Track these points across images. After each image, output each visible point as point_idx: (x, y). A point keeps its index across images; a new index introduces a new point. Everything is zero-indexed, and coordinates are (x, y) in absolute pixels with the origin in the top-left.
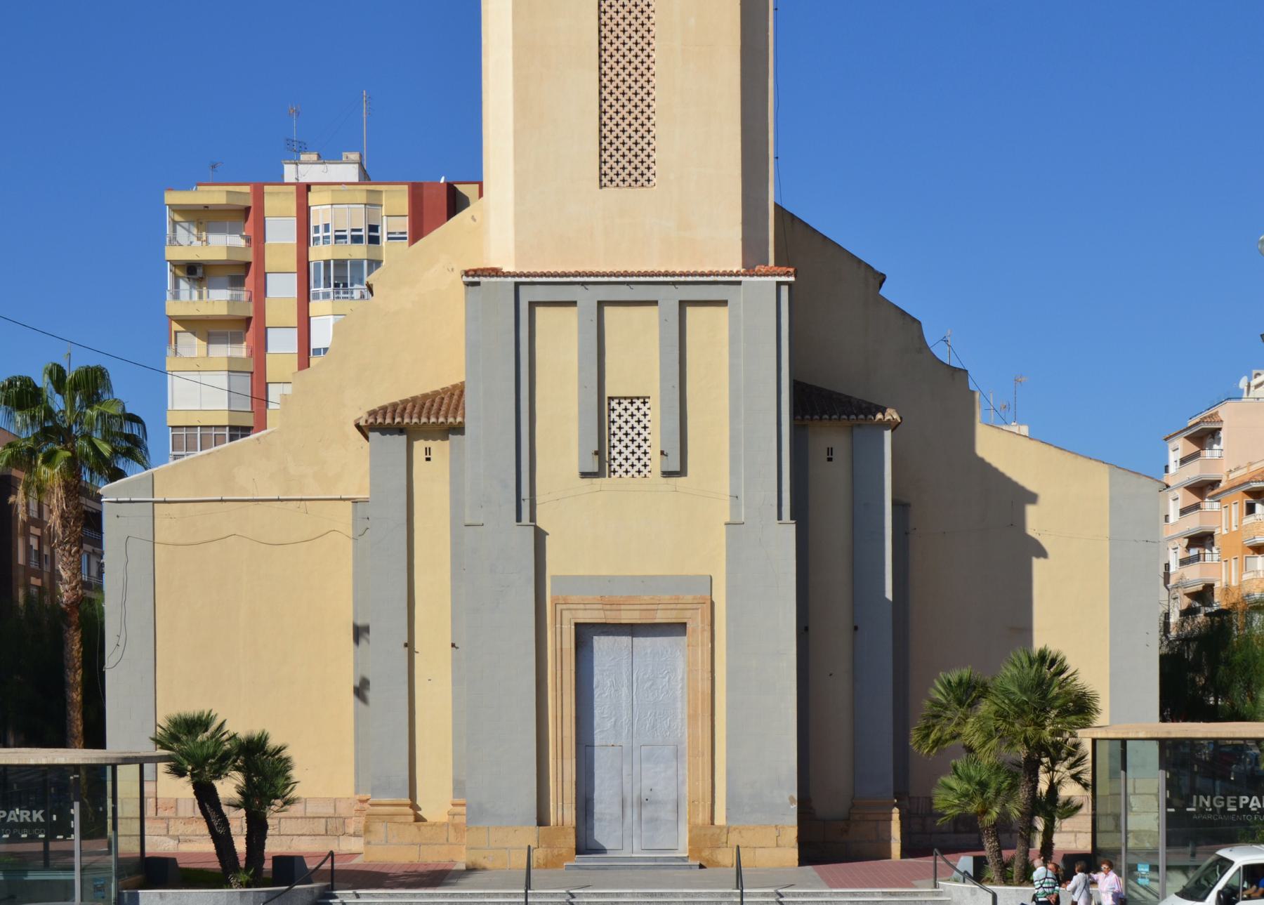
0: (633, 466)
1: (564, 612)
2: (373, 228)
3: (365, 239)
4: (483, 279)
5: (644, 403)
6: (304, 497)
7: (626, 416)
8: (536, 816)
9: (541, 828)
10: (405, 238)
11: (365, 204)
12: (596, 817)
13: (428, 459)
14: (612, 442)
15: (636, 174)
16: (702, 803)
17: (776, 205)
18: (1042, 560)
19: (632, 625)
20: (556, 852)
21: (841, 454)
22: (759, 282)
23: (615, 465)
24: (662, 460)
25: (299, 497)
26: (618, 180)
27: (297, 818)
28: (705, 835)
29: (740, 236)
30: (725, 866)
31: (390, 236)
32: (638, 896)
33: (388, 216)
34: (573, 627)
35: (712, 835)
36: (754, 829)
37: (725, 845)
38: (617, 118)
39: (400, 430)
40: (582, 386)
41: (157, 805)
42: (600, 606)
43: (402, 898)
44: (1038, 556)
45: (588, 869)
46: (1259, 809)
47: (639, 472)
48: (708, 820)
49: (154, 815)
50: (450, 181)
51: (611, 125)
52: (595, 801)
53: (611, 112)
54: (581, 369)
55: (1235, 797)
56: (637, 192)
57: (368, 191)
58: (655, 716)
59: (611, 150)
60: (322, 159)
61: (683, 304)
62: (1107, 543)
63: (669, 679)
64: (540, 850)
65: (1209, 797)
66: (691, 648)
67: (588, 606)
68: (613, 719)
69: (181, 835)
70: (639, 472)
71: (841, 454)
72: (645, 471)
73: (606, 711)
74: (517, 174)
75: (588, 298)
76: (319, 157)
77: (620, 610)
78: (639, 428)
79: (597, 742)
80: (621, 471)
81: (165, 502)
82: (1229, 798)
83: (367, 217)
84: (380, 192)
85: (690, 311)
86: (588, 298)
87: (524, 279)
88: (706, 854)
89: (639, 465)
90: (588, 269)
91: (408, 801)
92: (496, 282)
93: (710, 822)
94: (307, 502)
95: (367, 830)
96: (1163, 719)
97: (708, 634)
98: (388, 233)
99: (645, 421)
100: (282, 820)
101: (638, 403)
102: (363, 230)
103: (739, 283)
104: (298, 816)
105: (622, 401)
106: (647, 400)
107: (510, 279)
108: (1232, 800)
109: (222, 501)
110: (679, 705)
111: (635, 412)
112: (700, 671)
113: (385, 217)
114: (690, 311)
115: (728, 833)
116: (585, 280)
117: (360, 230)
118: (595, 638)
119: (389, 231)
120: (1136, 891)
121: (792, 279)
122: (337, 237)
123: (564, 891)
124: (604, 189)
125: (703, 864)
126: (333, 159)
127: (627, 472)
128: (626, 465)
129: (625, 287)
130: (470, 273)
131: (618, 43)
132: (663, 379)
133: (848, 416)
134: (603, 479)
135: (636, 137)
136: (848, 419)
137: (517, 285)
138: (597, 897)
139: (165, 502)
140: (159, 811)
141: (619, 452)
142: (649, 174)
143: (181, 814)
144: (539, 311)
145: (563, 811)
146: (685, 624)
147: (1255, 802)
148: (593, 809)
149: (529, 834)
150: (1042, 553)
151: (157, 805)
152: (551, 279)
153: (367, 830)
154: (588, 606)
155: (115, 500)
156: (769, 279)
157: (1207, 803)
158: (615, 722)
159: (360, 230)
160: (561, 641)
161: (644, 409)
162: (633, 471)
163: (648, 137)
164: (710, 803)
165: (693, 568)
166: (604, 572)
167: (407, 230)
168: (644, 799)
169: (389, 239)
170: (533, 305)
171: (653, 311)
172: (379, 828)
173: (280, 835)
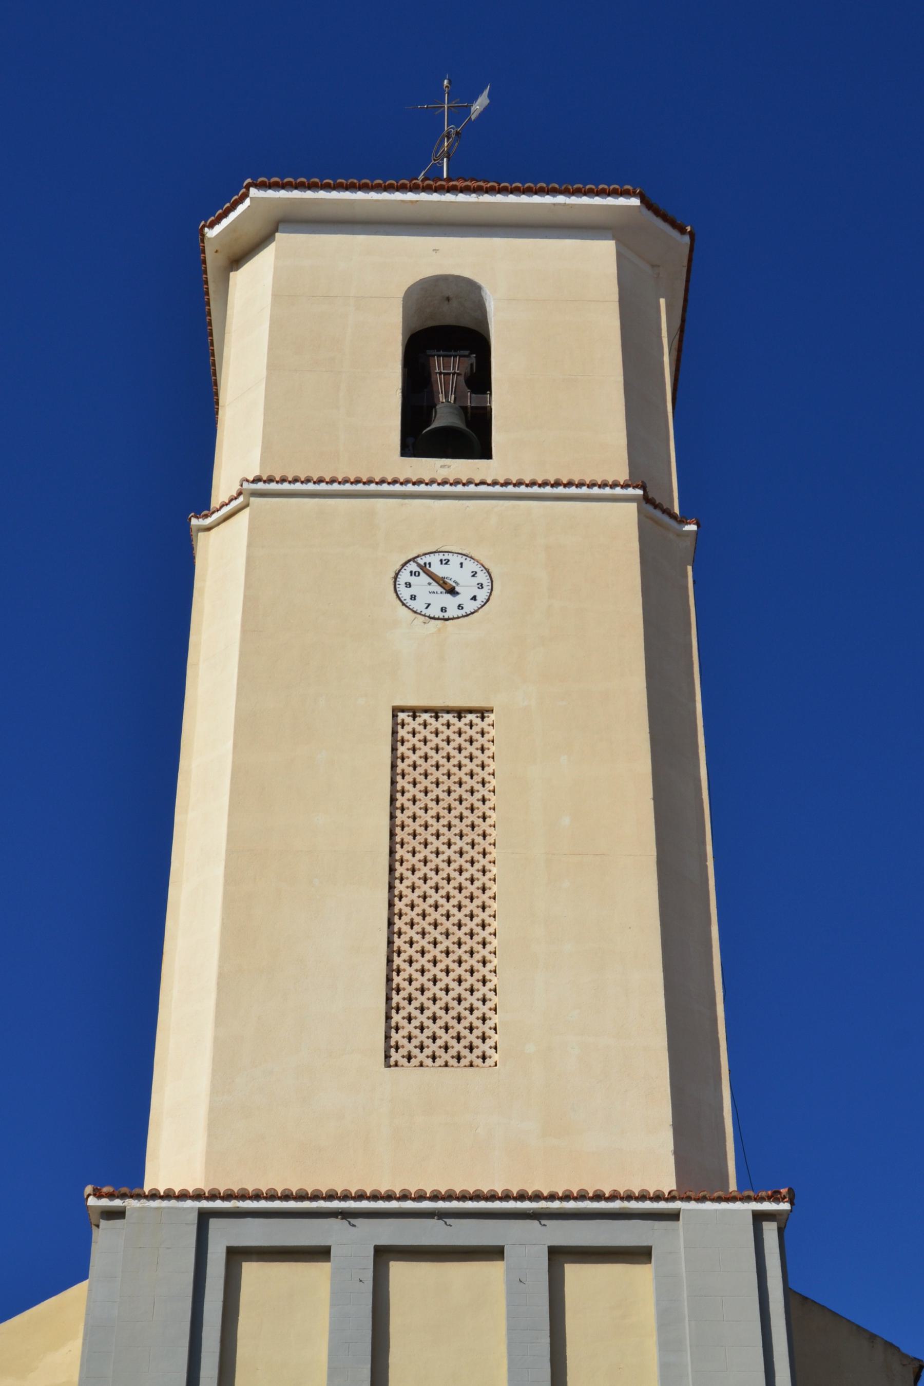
29: (671, 1146)
51: (408, 971)
56: (457, 1075)
74: (219, 1044)
85: (398, 1270)
87: (219, 1204)
103: (674, 1216)
107: (189, 1204)
110: (441, 395)
114: (398, 1270)
118: (566, 1265)
121: (785, 1206)
129: (434, 1222)
142: (482, 1047)
144: (251, 1271)
156: (738, 1205)
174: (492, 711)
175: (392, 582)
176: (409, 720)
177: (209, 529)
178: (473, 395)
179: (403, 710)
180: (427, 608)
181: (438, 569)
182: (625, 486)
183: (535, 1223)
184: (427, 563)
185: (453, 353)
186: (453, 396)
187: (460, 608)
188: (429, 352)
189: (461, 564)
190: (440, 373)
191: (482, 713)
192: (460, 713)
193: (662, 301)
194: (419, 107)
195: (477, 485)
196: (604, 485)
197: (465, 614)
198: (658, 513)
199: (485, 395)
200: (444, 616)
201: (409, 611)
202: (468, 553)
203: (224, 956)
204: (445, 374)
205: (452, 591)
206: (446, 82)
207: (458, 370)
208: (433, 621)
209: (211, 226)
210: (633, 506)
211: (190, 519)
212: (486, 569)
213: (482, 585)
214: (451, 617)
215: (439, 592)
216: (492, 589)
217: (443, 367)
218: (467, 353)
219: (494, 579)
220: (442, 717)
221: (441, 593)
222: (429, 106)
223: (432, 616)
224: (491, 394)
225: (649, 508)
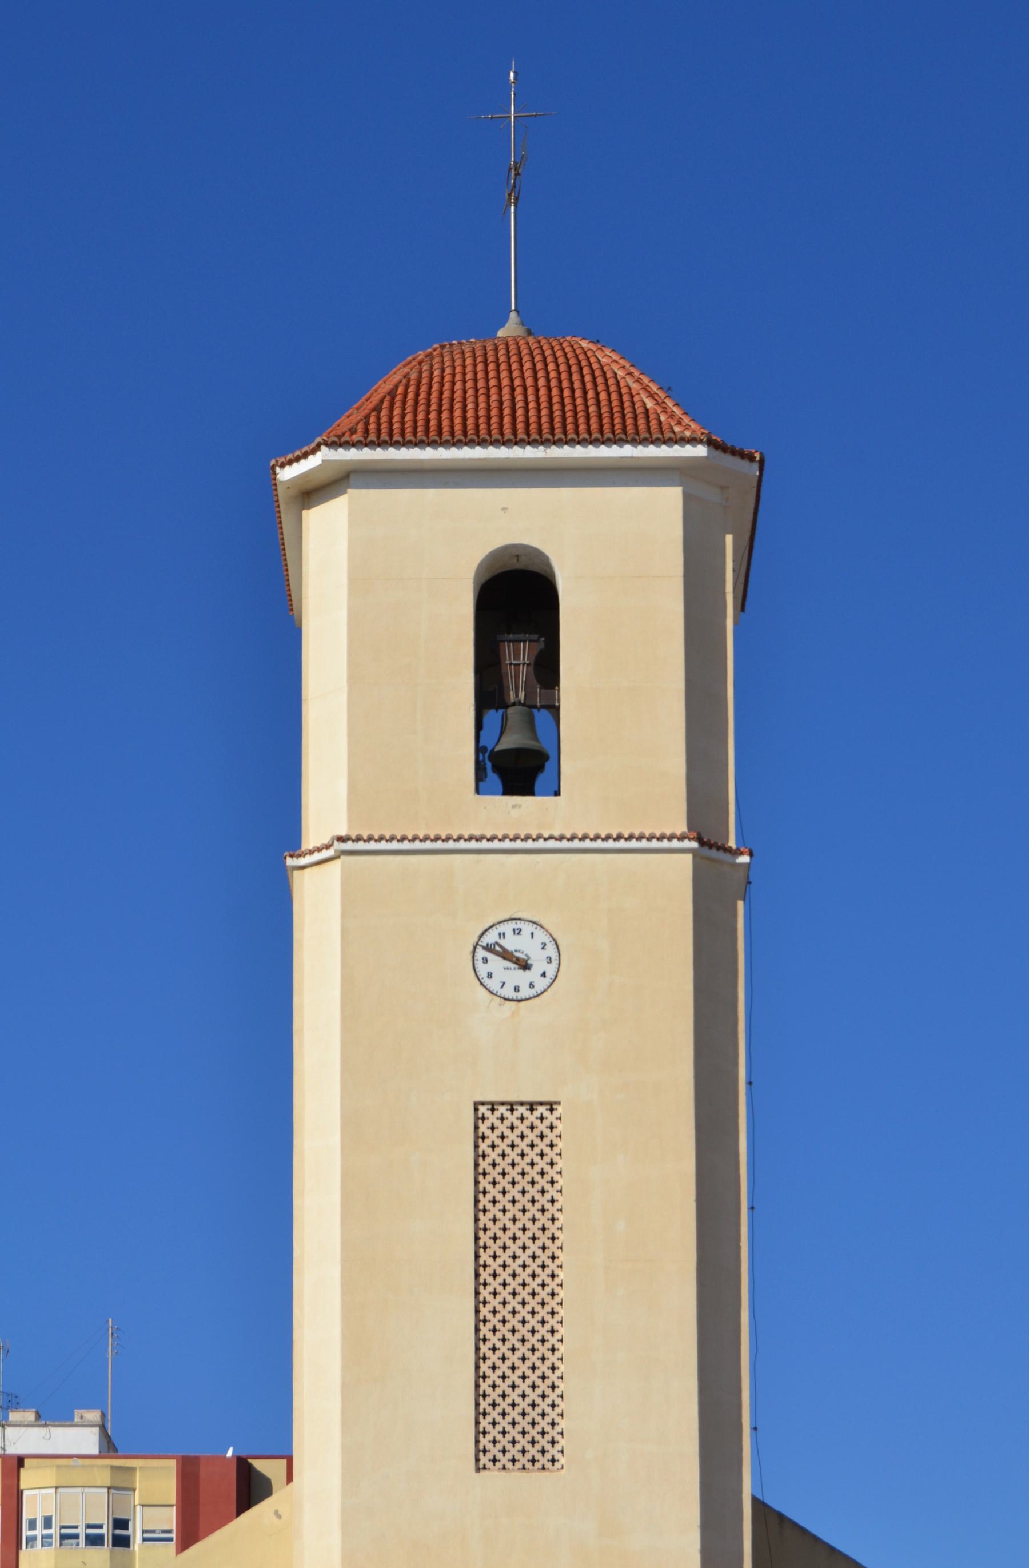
2: (121, 1524)
3: (108, 1540)
10: (171, 1540)
11: (109, 1488)
15: (533, 1451)
17: (758, 1504)
29: (697, 1545)
31: (146, 1535)
38: (504, 1368)
50: (243, 1454)
51: (494, 1377)
56: (534, 1478)
59: (494, 1414)
60: (42, 1419)
74: (345, 1448)
76: (38, 1416)
83: (111, 1505)
84: (132, 1470)
98: (144, 1532)
102: (105, 1527)
110: (511, 693)
113: (138, 1509)
117: (100, 1526)
122: (63, 1537)
124: (483, 1473)
131: (504, 1257)
135: (533, 1396)
142: (553, 1451)
159: (100, 1526)
163: (553, 1396)
174: (559, 1103)
175: (470, 957)
176: (488, 1114)
177: (303, 868)
178: (543, 691)
179: (483, 1104)
180: (502, 987)
181: (511, 943)
182: (682, 838)
184: (502, 933)
185: (521, 636)
186: (523, 693)
187: (532, 986)
188: (499, 637)
189: (532, 934)
190: (511, 664)
191: (551, 1106)
192: (532, 1106)
193: (729, 539)
194: (483, 117)
195: (545, 840)
196: (660, 838)
197: (535, 994)
198: (714, 853)
199: (554, 691)
200: (517, 997)
201: (486, 991)
202: (538, 920)
203: (345, 1367)
204: (515, 665)
205: (525, 965)
206: (512, 74)
207: (528, 660)
208: (508, 1003)
209: (282, 466)
210: (689, 857)
211: (285, 858)
212: (554, 940)
213: (550, 959)
214: (523, 998)
215: (513, 968)
216: (559, 965)
217: (514, 655)
218: (535, 637)
219: (561, 953)
220: (517, 1109)
221: (515, 969)
222: (494, 116)
223: (506, 997)
224: (559, 690)
225: (706, 851)
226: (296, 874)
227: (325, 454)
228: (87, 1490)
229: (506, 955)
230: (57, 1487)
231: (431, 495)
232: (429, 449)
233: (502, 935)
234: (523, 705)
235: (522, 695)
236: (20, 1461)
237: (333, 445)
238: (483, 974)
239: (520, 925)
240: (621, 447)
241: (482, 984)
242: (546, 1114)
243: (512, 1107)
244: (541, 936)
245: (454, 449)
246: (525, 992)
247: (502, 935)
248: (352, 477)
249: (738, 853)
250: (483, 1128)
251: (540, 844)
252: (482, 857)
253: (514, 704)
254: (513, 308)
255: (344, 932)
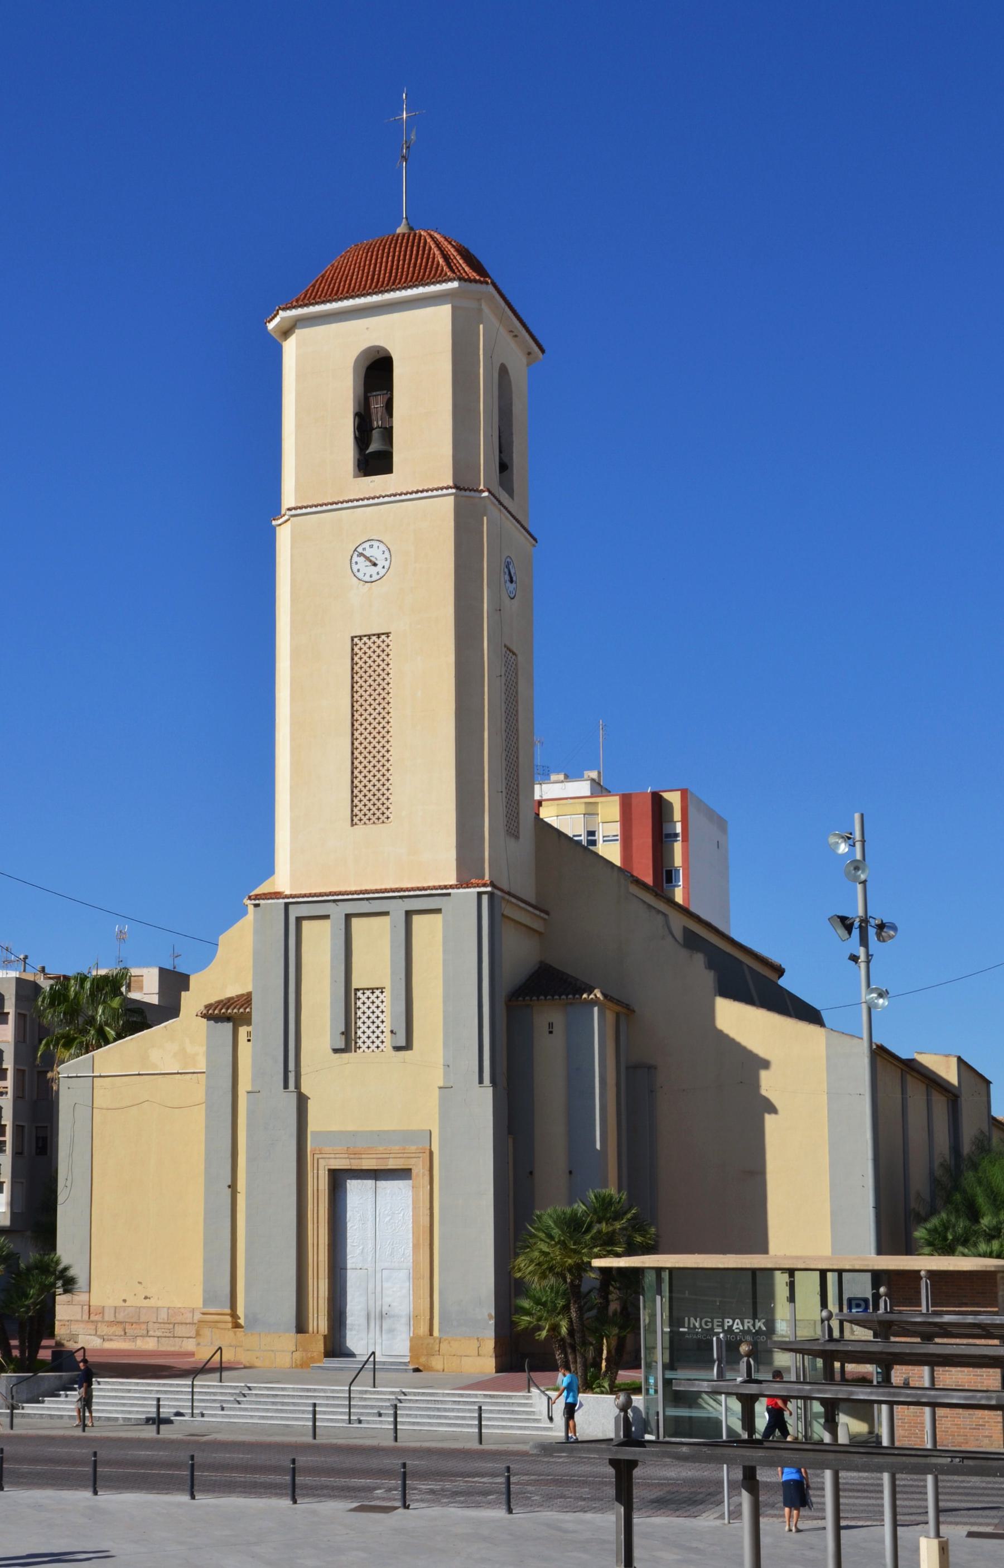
0: (373, 1042)
1: (320, 1160)
2: (591, 833)
4: (261, 902)
5: (382, 992)
6: (196, 1071)
7: (368, 1003)
8: (294, 1325)
9: (299, 1334)
10: (617, 840)
11: (584, 814)
12: (348, 1327)
13: (249, 1040)
14: (358, 1024)
15: (378, 814)
16: (423, 1318)
18: (773, 1116)
19: (375, 1171)
20: (309, 1355)
21: (559, 1028)
22: (464, 893)
23: (360, 1042)
24: (392, 1037)
25: (192, 1071)
26: (365, 819)
27: (186, 1324)
28: (422, 1344)
29: (455, 857)
30: (437, 1371)
31: (605, 839)
32: (297, 1391)
33: (603, 823)
34: (327, 1172)
35: (428, 1344)
36: (460, 1341)
37: (437, 1353)
39: (228, 1019)
40: (334, 982)
41: (89, 1311)
42: (346, 1156)
43: (129, 1385)
44: (769, 1113)
45: (328, 1370)
46: (741, 1331)
47: (378, 1047)
48: (427, 1332)
49: (87, 1319)
50: (656, 790)
52: (347, 1314)
53: (360, 767)
54: (333, 967)
55: (721, 1320)
57: (586, 803)
58: (392, 1245)
61: (409, 914)
62: (825, 1097)
63: (404, 1214)
64: (298, 1353)
65: (698, 1319)
66: (415, 1189)
67: (337, 1156)
68: (361, 1247)
69: (105, 1335)
70: (378, 1047)
71: (559, 1028)
72: (382, 1047)
73: (355, 1241)
75: (338, 912)
76: (567, 777)
77: (362, 1158)
78: (378, 1012)
79: (349, 1266)
80: (364, 1047)
81: (100, 1076)
82: (715, 1320)
83: (586, 824)
85: (355, 922)
86: (397, 909)
87: (291, 900)
88: (423, 1360)
89: (378, 1042)
90: (343, 889)
91: (228, 1311)
92: (271, 903)
93: (429, 1333)
94: (199, 1075)
95: (198, 1334)
96: (880, 1252)
97: (427, 1178)
98: (604, 837)
99: (382, 1007)
100: (176, 1325)
101: (377, 992)
102: (583, 836)
103: (449, 894)
104: (188, 1322)
105: (365, 991)
106: (384, 990)
108: (718, 1322)
109: (139, 1075)
111: (375, 1000)
112: (421, 1208)
113: (601, 824)
114: (416, 919)
115: (440, 1343)
116: (400, 894)
117: (580, 836)
118: (348, 1181)
119: (605, 835)
120: (708, 1404)
123: (243, 1385)
124: (355, 827)
125: (421, 1368)
126: (579, 777)
127: (369, 1047)
128: (368, 1042)
130: (252, 897)
132: (393, 973)
133: (560, 997)
134: (350, 1054)
136: (560, 999)
137: (287, 905)
138: (268, 1390)
139: (100, 1076)
140: (91, 1315)
141: (363, 1030)
143: (106, 1318)
145: (319, 1322)
146: (410, 1170)
147: (738, 1324)
148: (346, 1321)
149: (289, 1339)
150: (773, 1110)
151: (89, 1311)
152: (310, 899)
153: (198, 1334)
154: (337, 1156)
155: (66, 1075)
157: (697, 1325)
158: (363, 1248)
159: (580, 836)
160: (319, 1185)
161: (382, 997)
162: (373, 1047)
164: (428, 1317)
165: (417, 1124)
166: (351, 1127)
167: (619, 833)
168: (384, 1313)
169: (604, 841)
170: (299, 920)
171: (386, 920)
172: (206, 1332)
173: (174, 1337)
176: (358, 642)
177: (280, 525)
179: (356, 637)
181: (367, 553)
183: (400, 900)
185: (378, 393)
191: (388, 635)
192: (379, 636)
198: (467, 493)
205: (375, 565)
206: (404, 95)
208: (367, 584)
209: (269, 322)
210: (452, 497)
218: (385, 392)
225: (463, 493)
226: (277, 528)
227: (282, 314)
228: (573, 816)
229: (367, 558)
230: (557, 816)
231: (334, 327)
232: (328, 304)
233: (364, 549)
234: (381, 428)
235: (380, 423)
236: (540, 803)
237: (284, 309)
238: (355, 570)
239: (372, 543)
240: (417, 288)
241: (355, 575)
242: (386, 639)
243: (369, 637)
244: (382, 547)
245: (340, 302)
246: (375, 577)
247: (364, 549)
248: (298, 323)
249: (482, 491)
250: (356, 649)
251: (381, 500)
252: (355, 510)
253: (376, 428)
254: (404, 216)
255: (292, 556)
